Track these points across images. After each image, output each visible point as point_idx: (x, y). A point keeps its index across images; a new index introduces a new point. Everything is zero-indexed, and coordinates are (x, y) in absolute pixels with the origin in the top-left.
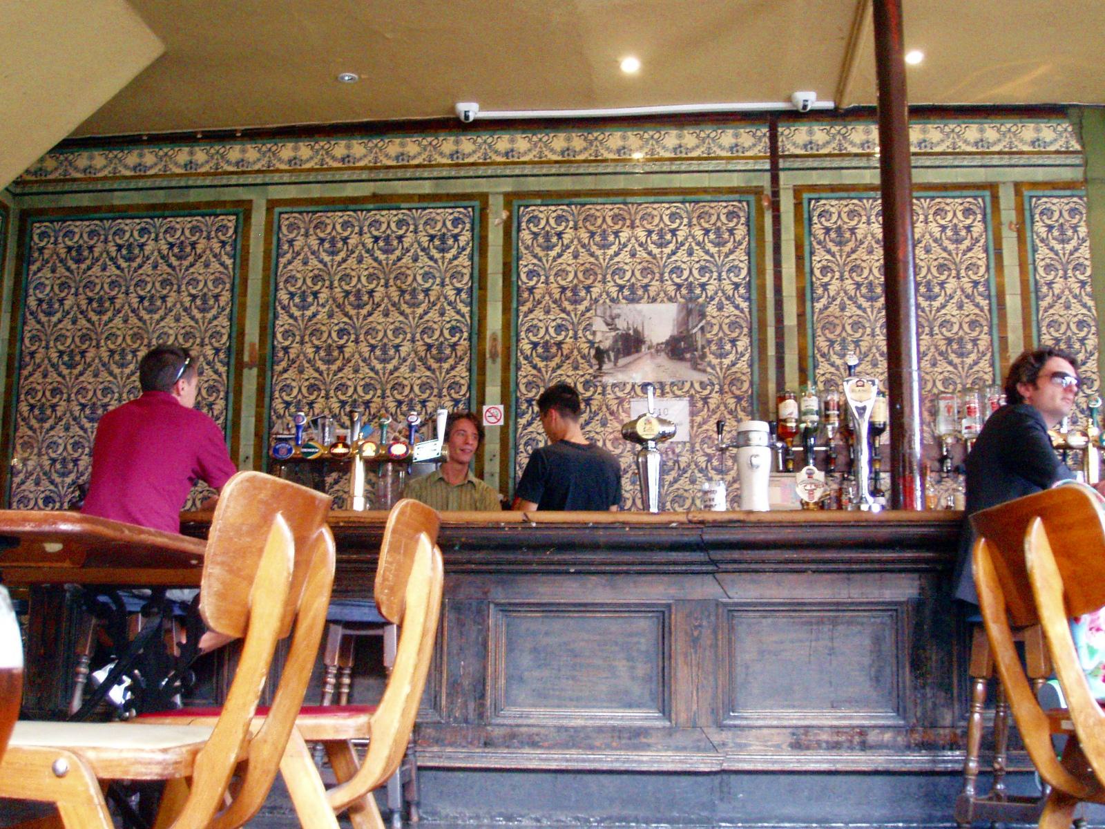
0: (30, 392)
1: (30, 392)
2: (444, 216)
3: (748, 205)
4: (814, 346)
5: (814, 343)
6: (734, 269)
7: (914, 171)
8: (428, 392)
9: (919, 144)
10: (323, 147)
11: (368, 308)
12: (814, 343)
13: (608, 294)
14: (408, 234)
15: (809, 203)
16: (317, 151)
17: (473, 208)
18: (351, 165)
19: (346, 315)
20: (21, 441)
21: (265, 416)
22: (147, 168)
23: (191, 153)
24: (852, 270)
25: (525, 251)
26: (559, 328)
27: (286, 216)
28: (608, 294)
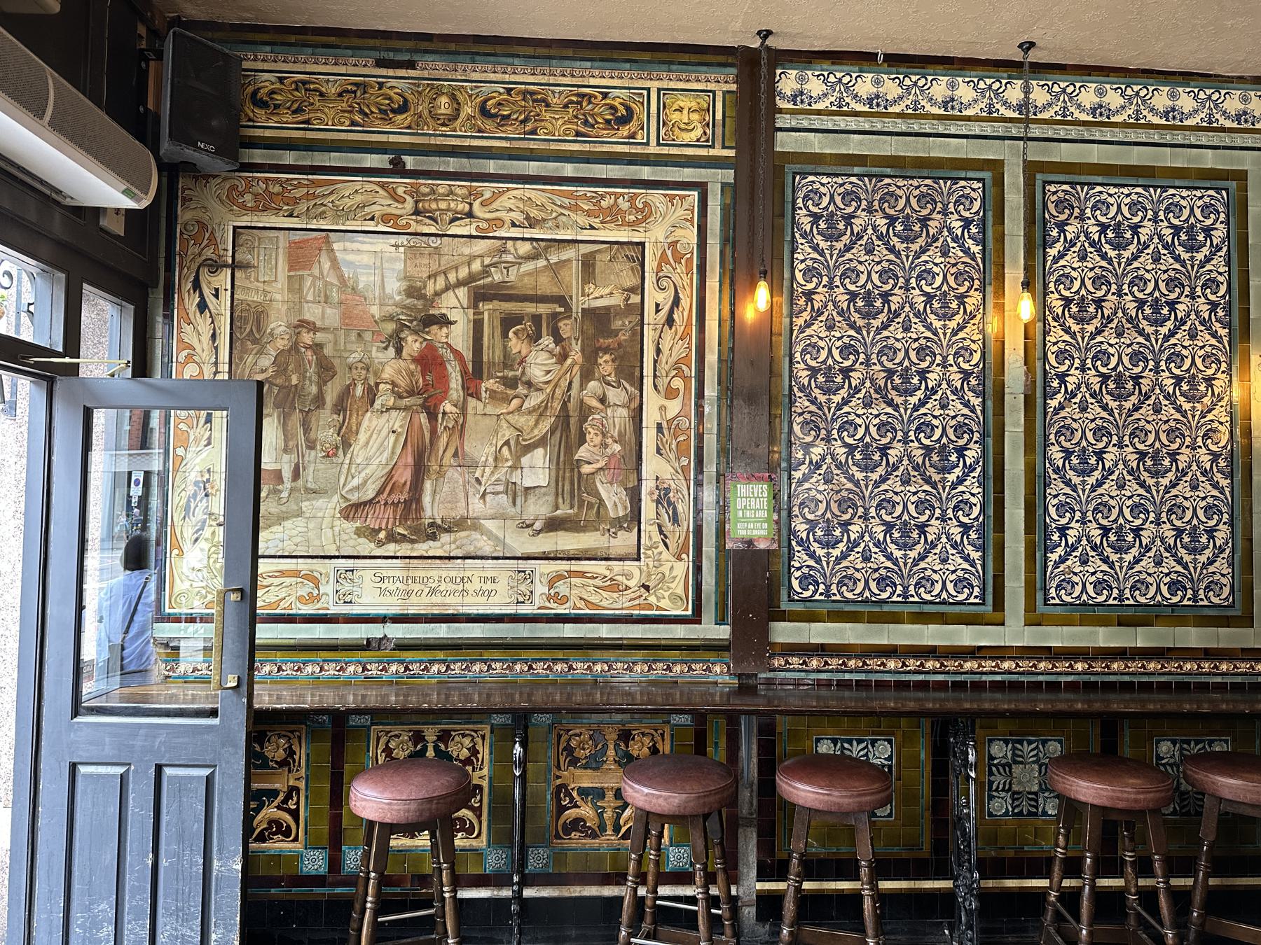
0: (1063, 431)
1: (1063, 431)
2: (1190, 200)
3: (1050, 183)
4: (790, 377)
5: (791, 371)
6: (1211, 284)
7: (779, 134)
8: (966, 436)
9: (794, 98)
10: (1137, 94)
11: (883, 317)
12: (791, 371)
13: (1197, 313)
14: (1145, 223)
15: (979, 180)
16: (1057, 95)
17: (1046, 183)
18: (882, 109)
19: (1141, 333)
20: (1055, 501)
21: (1039, 469)
22: (1183, 115)
23: (952, 86)
24: (920, 277)
25: (801, 241)
26: (1136, 357)
27: (1053, 189)
28: (1197, 313)
